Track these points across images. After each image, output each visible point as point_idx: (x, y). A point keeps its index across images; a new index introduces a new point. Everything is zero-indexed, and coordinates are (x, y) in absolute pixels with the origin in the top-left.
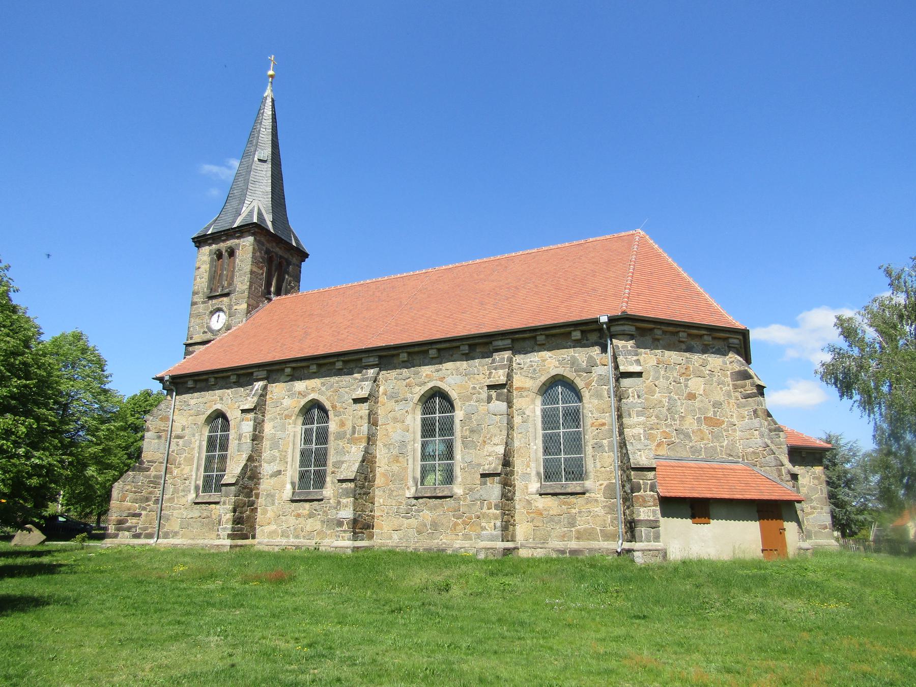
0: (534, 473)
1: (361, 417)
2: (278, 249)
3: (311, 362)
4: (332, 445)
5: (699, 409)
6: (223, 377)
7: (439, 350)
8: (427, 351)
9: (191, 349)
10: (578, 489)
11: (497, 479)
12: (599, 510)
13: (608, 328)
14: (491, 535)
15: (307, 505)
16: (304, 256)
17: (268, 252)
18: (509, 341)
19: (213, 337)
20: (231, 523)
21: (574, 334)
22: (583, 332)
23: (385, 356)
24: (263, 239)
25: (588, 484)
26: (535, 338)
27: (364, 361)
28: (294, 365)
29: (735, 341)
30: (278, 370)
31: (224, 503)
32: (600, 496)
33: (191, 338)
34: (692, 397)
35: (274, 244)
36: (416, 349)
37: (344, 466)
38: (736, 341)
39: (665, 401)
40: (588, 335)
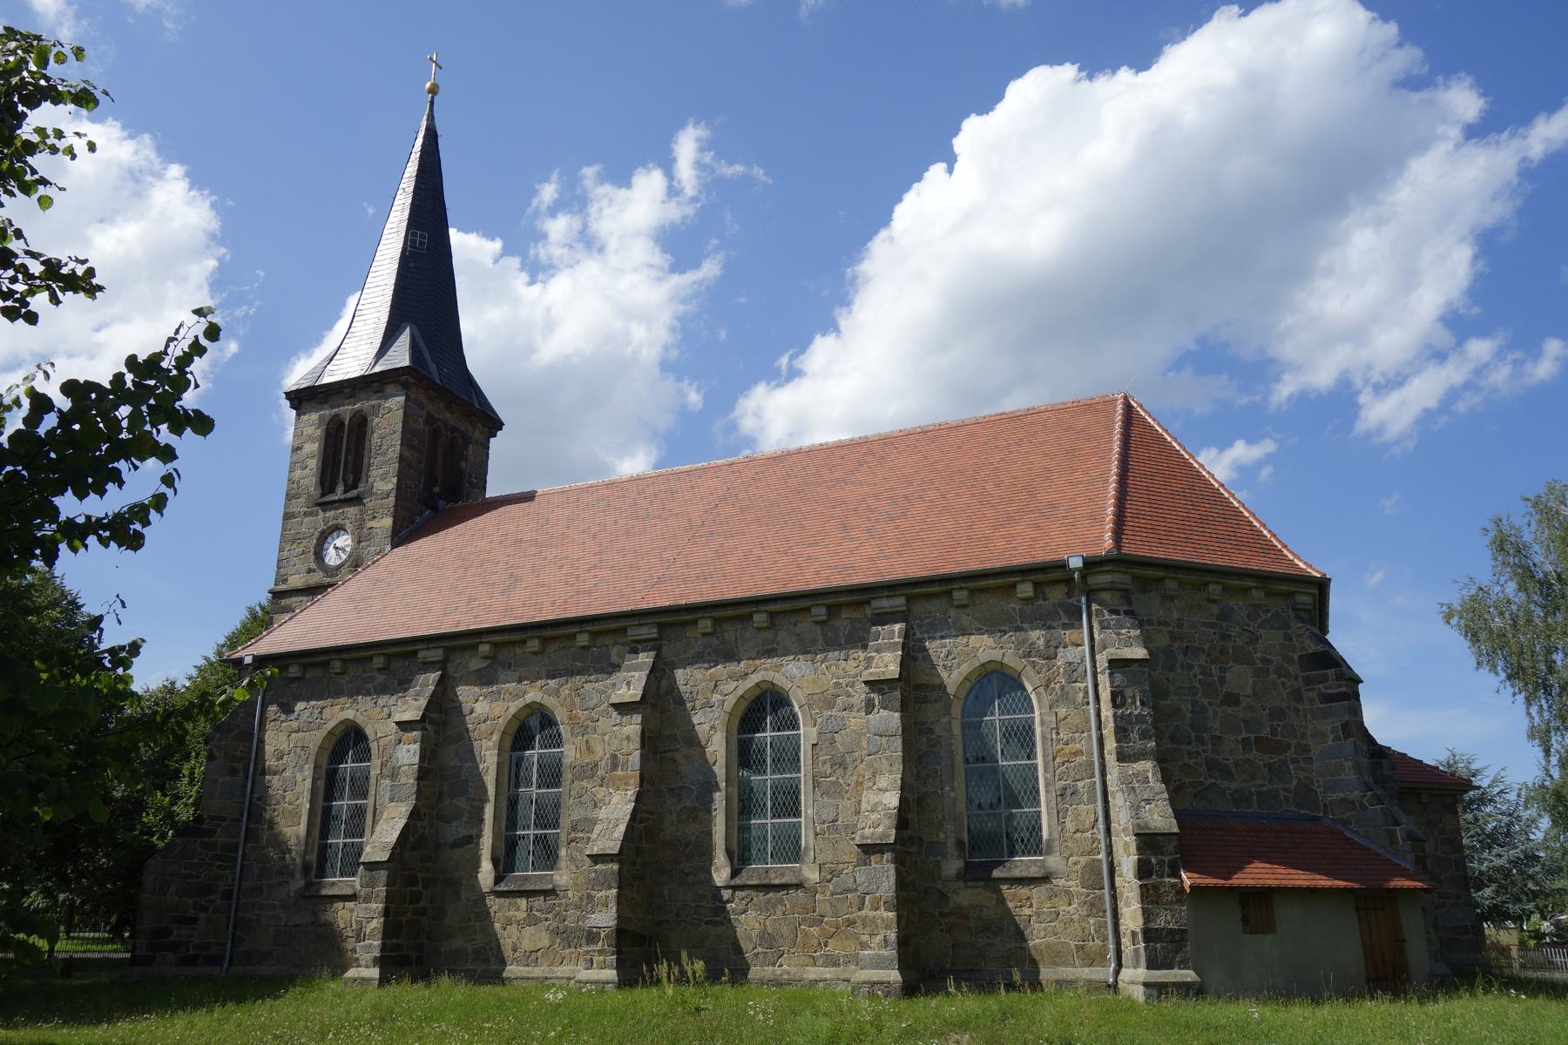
0: (951, 842)
1: (628, 738)
2: (448, 415)
3: (529, 634)
4: (569, 788)
5: (1246, 722)
6: (358, 660)
7: (772, 615)
8: (750, 616)
9: (284, 602)
10: (1034, 872)
11: (888, 856)
12: (1074, 909)
13: (1084, 577)
14: (879, 957)
15: (523, 903)
16: (498, 425)
17: (430, 420)
18: (901, 601)
19: (327, 580)
20: (380, 936)
21: (1020, 587)
22: (1036, 585)
23: (671, 625)
24: (422, 397)
25: (1053, 861)
26: (949, 594)
27: (630, 632)
28: (496, 638)
29: (1305, 599)
30: (465, 648)
31: (368, 899)
32: (1074, 885)
33: (285, 581)
34: (1232, 699)
35: (442, 405)
36: (730, 612)
37: (598, 828)
38: (1307, 599)
39: (1186, 708)
40: (1047, 590)
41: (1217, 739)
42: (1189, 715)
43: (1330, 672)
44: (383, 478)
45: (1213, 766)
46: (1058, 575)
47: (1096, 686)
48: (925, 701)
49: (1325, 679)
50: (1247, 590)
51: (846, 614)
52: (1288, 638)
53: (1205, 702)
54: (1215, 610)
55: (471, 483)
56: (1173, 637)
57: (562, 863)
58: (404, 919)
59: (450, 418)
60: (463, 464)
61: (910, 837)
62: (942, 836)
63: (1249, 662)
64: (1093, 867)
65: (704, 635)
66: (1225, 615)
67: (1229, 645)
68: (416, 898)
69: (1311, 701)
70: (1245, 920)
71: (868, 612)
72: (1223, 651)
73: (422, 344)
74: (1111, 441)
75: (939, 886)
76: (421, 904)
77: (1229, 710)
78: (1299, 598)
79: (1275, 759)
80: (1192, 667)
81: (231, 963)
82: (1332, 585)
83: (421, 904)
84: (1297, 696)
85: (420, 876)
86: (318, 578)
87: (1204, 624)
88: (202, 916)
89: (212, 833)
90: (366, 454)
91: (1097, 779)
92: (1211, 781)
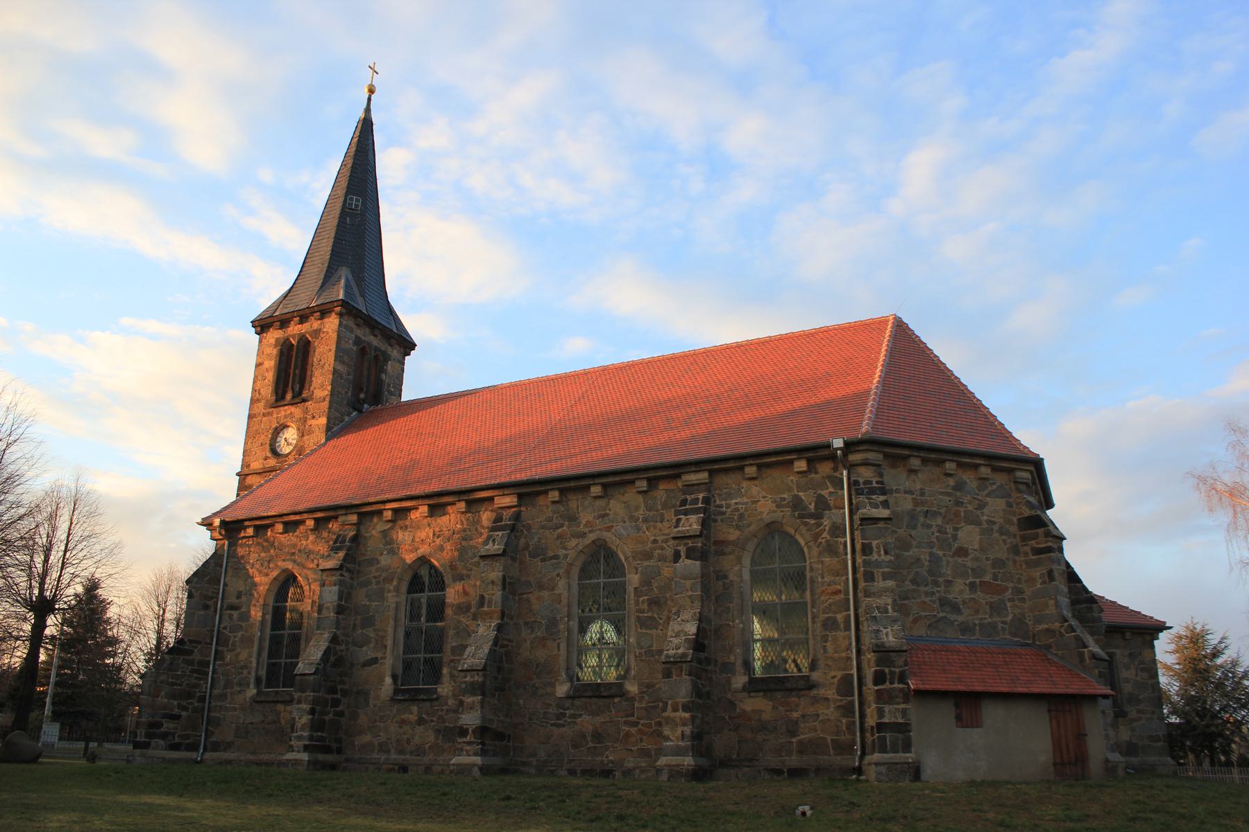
0: (739, 662)
12: (830, 712)
13: (845, 454)
14: (678, 746)
16: (412, 346)
17: (358, 341)
23: (529, 494)
24: (351, 323)
32: (831, 693)
34: (962, 552)
35: (367, 330)
38: (1026, 475)
39: (925, 558)
40: (818, 466)
41: (949, 583)
42: (927, 563)
43: (1041, 531)
44: (321, 383)
45: (944, 602)
46: (826, 452)
47: (853, 540)
48: (722, 553)
49: (1036, 537)
50: (977, 466)
51: (663, 486)
52: (1009, 505)
53: (940, 553)
54: (951, 482)
55: (389, 392)
56: (916, 503)
57: (446, 679)
58: (327, 718)
59: (375, 341)
60: (383, 376)
61: (706, 659)
62: (732, 657)
63: (979, 523)
64: (847, 680)
65: (553, 502)
66: (960, 486)
67: (962, 509)
68: (336, 703)
69: (1026, 554)
70: (958, 718)
71: (680, 484)
72: (957, 514)
73: (353, 283)
74: (879, 353)
75: (729, 696)
76: (340, 708)
77: (960, 560)
78: (1019, 474)
79: (996, 598)
80: (929, 526)
81: (205, 750)
82: (1045, 462)
83: (340, 708)
84: (1015, 550)
85: (339, 687)
86: (272, 462)
87: (942, 493)
88: (184, 713)
89: (190, 652)
90: (309, 367)
91: (852, 612)
92: (941, 615)
